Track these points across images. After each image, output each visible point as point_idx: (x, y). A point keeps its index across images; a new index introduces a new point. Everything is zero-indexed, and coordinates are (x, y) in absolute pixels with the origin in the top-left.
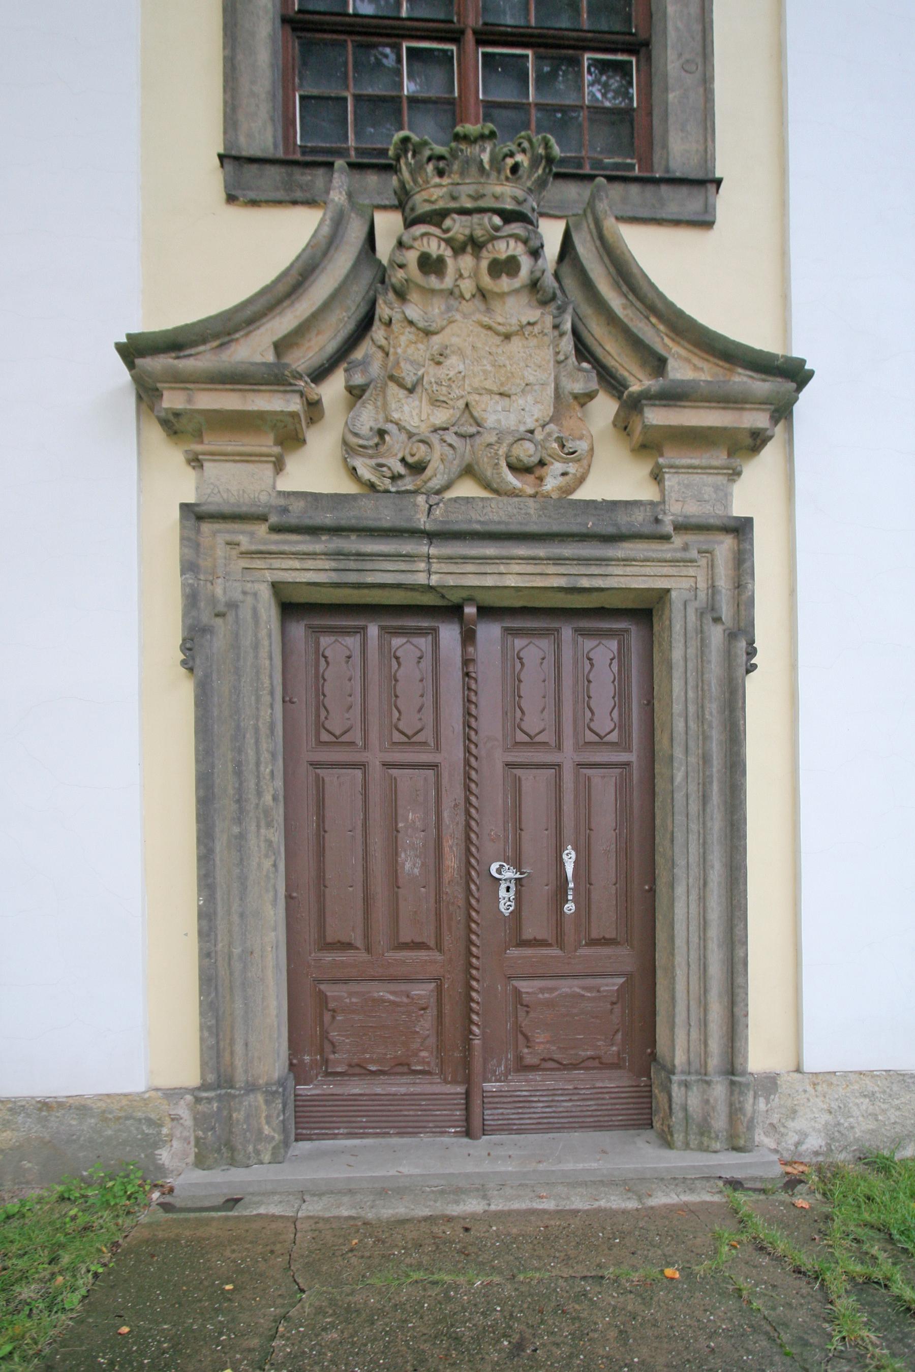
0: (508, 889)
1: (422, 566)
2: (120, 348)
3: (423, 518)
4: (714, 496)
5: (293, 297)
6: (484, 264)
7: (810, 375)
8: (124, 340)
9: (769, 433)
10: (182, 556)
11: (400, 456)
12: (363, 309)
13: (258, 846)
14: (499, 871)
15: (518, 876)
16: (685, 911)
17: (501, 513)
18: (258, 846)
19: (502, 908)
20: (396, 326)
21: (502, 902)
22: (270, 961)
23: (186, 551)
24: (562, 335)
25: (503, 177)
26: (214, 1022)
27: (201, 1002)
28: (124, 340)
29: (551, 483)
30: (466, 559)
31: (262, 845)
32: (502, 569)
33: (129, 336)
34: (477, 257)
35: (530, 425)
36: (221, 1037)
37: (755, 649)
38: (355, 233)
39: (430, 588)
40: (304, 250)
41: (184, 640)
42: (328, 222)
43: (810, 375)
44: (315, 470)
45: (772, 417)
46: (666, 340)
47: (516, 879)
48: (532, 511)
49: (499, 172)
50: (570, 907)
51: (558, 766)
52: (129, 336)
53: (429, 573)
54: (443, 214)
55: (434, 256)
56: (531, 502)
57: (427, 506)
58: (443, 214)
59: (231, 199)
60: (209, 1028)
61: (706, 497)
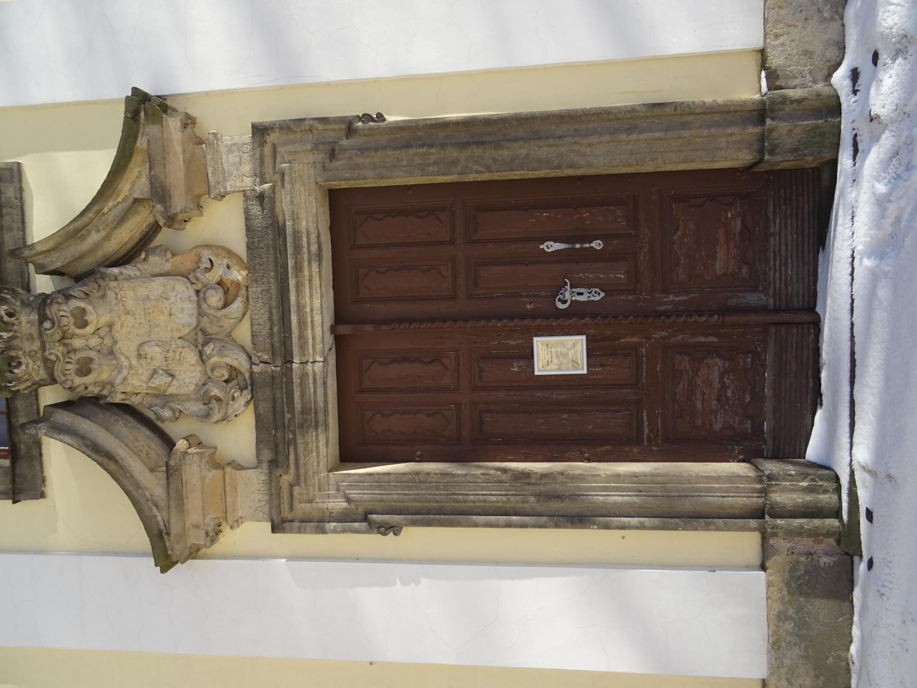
0: (579, 294)
1: (309, 367)
2: (163, 571)
3: (278, 369)
4: (236, 153)
5: (118, 458)
6: (78, 331)
7: (135, 90)
8: (159, 568)
9: (182, 116)
10: (312, 533)
11: (224, 384)
12: (116, 410)
13: (546, 484)
14: (564, 302)
15: (568, 287)
16: (601, 158)
17: (262, 311)
18: (546, 484)
19: (597, 298)
20: (129, 389)
21: (592, 298)
22: (860, 583)
23: (309, 530)
24: (121, 274)
25: (16, 322)
26: (702, 520)
27: (684, 529)
28: (159, 568)
29: (238, 275)
30: (302, 337)
31: (544, 481)
32: (308, 309)
33: (156, 565)
34: (73, 336)
35: (192, 293)
36: (384, 328)
37: (364, 115)
38: (64, 418)
39: (325, 361)
40: (83, 452)
41: (379, 533)
42: (61, 437)
43: (135, 90)
44: (238, 435)
45: (171, 115)
46: (120, 199)
47: (571, 288)
48: (259, 289)
49: (13, 324)
50: (597, 245)
51: (452, 242)
52: (156, 565)
53: (314, 362)
54: (46, 360)
55: (77, 366)
56: (252, 289)
57: (261, 364)
58: (46, 360)
59: (42, 495)
60: (707, 524)
61: (237, 159)
